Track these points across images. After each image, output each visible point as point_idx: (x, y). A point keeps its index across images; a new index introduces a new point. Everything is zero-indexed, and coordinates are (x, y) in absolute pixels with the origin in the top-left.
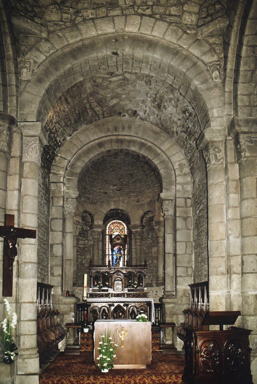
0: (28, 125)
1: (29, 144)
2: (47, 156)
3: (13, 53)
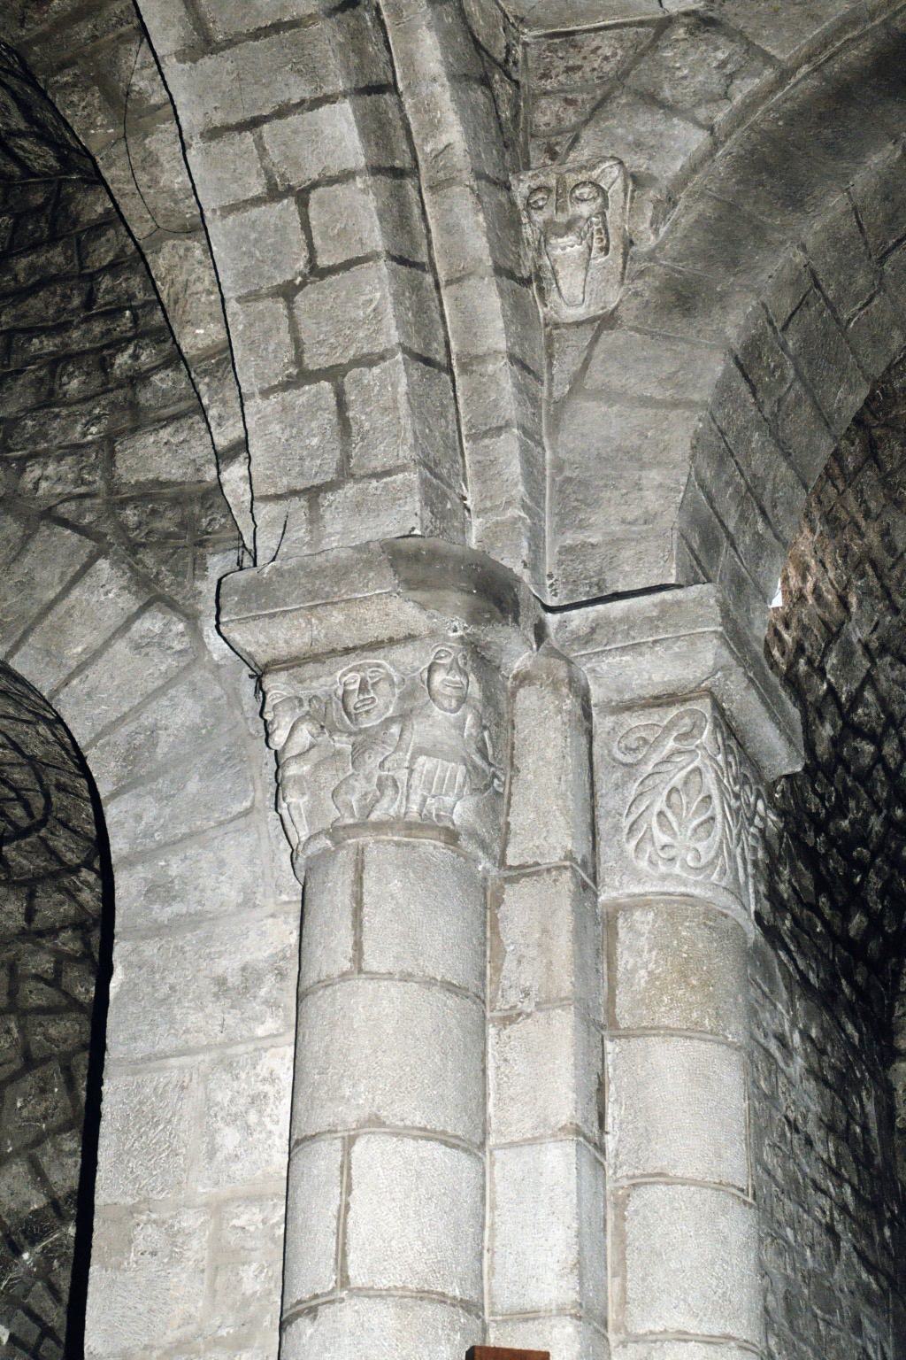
0: (621, 620)
1: (644, 761)
2: (847, 918)
3: (472, 136)
